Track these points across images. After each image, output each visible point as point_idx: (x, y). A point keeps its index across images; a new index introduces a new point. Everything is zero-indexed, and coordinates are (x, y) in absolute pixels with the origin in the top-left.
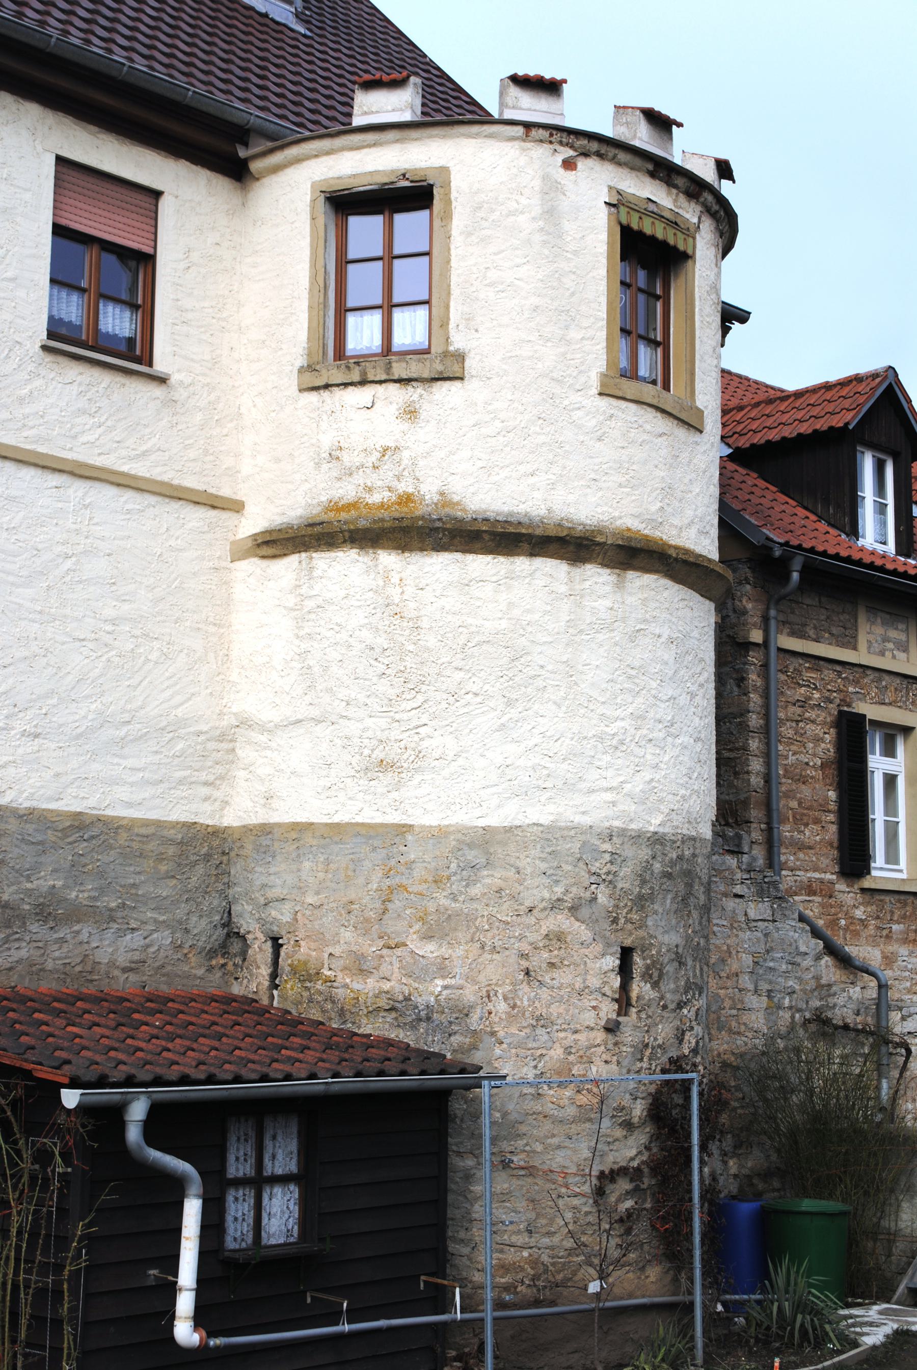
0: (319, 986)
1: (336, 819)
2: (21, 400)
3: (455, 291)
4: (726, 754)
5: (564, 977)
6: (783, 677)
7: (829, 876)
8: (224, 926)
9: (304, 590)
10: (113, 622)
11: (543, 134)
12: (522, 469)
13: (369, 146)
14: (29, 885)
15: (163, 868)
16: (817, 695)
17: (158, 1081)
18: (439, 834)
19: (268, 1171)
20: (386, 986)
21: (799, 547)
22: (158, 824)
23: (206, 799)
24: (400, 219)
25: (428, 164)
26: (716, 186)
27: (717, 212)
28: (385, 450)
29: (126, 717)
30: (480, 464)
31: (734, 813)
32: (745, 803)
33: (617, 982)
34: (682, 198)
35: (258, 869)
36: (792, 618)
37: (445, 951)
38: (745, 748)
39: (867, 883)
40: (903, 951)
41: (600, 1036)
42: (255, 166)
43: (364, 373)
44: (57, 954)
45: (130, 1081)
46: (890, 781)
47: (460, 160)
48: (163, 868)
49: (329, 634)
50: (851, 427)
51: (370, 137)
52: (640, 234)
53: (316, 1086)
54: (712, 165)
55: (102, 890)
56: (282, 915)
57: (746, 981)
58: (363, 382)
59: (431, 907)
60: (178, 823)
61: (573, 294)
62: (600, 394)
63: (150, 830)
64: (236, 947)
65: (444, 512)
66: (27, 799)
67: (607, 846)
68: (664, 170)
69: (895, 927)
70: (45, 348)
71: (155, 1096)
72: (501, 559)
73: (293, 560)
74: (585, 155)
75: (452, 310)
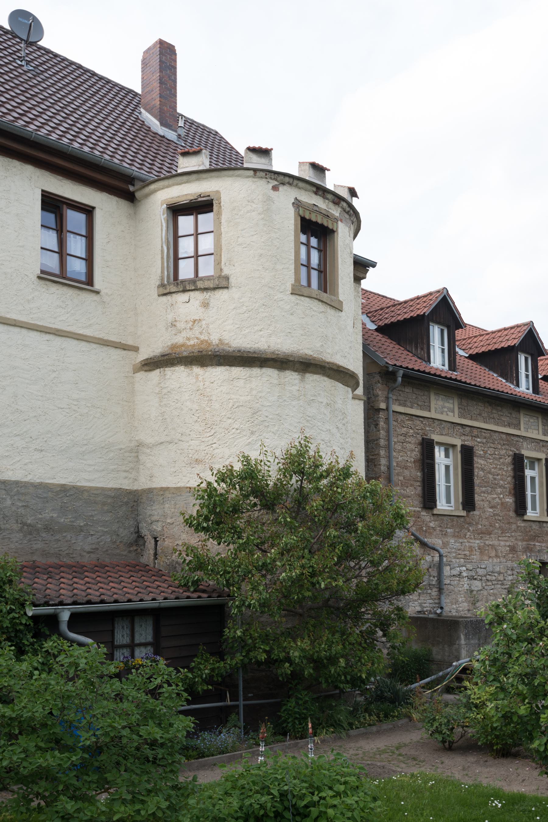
2: (28, 301)
4: (371, 457)
6: (395, 423)
7: (418, 509)
8: (136, 533)
9: (162, 385)
10: (77, 400)
11: (263, 174)
12: (256, 328)
13: (185, 183)
14: (40, 516)
15: (106, 508)
16: (411, 431)
17: (75, 603)
19: (137, 641)
21: (401, 366)
22: (103, 489)
23: (126, 478)
24: (200, 217)
25: (211, 190)
26: (350, 201)
27: (349, 211)
28: (194, 321)
29: (85, 442)
30: (237, 326)
34: (331, 205)
35: (148, 508)
36: (400, 398)
38: (379, 454)
39: (435, 512)
40: (452, 541)
42: (138, 195)
44: (55, 546)
45: (61, 603)
46: (533, 479)
47: (229, 190)
48: (106, 508)
49: (173, 404)
50: (426, 314)
51: (185, 178)
52: (310, 221)
53: (154, 604)
54: (347, 190)
56: (158, 527)
60: (112, 488)
61: (278, 248)
62: (292, 294)
63: (99, 492)
64: (141, 542)
65: (221, 347)
66: (38, 478)
69: (449, 530)
70: (39, 278)
71: (72, 610)
72: (247, 369)
74: (283, 184)
75: (223, 256)
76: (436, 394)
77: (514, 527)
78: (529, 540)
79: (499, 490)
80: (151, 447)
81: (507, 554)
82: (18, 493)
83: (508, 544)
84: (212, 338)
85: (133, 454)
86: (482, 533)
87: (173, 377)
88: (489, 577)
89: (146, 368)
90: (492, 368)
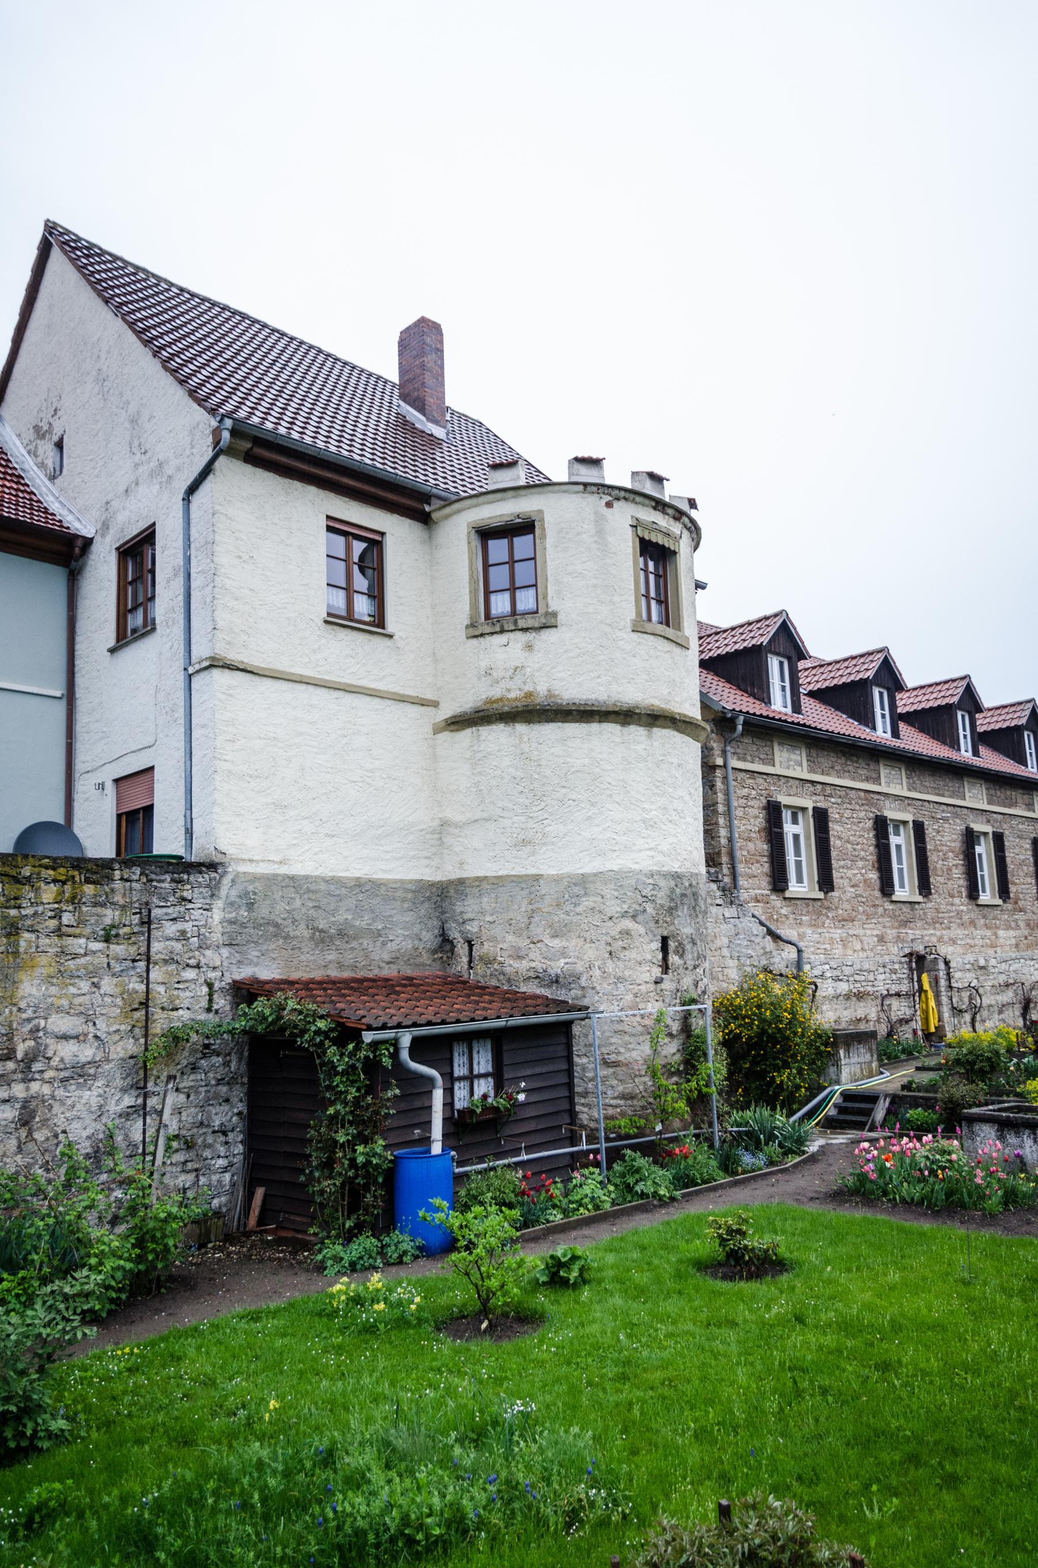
0: (496, 966)
1: (500, 873)
3: (550, 578)
5: (632, 954)
9: (475, 748)
11: (595, 489)
15: (406, 905)
17: (415, 1025)
18: (557, 880)
20: (533, 965)
22: (402, 881)
31: (713, 860)
32: (719, 853)
33: (660, 956)
34: (672, 521)
37: (565, 943)
38: (717, 823)
40: (809, 931)
41: (652, 987)
42: (434, 516)
43: (502, 627)
45: (399, 1026)
48: (406, 905)
51: (499, 496)
53: (500, 1023)
55: (374, 920)
56: (472, 928)
57: (725, 952)
58: (502, 631)
59: (556, 919)
67: (651, 881)
68: (660, 505)
70: (326, 622)
73: (468, 732)
74: (618, 499)
76: (780, 744)
77: (880, 910)
78: (900, 926)
79: (860, 864)
80: (460, 826)
81: (875, 946)
82: (309, 891)
83: (875, 933)
84: (539, 688)
85: (436, 836)
86: (844, 920)
87: (490, 737)
88: (857, 977)
89: (452, 727)
90: (838, 708)
